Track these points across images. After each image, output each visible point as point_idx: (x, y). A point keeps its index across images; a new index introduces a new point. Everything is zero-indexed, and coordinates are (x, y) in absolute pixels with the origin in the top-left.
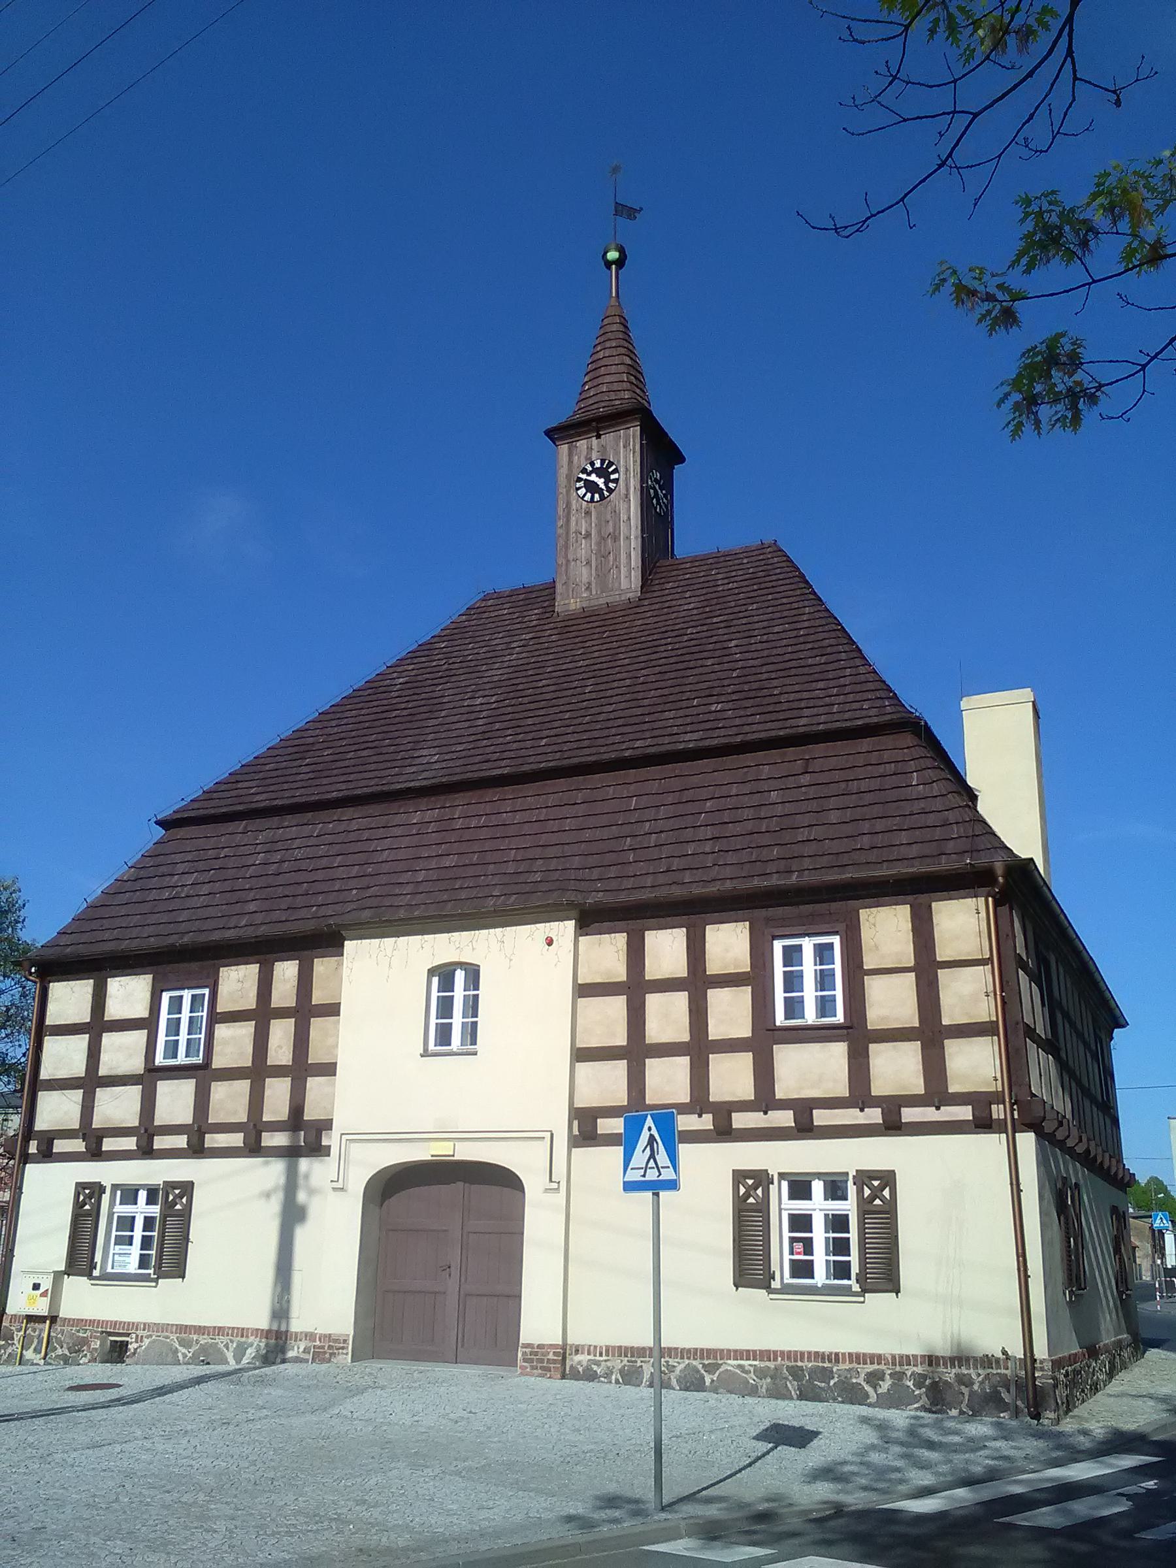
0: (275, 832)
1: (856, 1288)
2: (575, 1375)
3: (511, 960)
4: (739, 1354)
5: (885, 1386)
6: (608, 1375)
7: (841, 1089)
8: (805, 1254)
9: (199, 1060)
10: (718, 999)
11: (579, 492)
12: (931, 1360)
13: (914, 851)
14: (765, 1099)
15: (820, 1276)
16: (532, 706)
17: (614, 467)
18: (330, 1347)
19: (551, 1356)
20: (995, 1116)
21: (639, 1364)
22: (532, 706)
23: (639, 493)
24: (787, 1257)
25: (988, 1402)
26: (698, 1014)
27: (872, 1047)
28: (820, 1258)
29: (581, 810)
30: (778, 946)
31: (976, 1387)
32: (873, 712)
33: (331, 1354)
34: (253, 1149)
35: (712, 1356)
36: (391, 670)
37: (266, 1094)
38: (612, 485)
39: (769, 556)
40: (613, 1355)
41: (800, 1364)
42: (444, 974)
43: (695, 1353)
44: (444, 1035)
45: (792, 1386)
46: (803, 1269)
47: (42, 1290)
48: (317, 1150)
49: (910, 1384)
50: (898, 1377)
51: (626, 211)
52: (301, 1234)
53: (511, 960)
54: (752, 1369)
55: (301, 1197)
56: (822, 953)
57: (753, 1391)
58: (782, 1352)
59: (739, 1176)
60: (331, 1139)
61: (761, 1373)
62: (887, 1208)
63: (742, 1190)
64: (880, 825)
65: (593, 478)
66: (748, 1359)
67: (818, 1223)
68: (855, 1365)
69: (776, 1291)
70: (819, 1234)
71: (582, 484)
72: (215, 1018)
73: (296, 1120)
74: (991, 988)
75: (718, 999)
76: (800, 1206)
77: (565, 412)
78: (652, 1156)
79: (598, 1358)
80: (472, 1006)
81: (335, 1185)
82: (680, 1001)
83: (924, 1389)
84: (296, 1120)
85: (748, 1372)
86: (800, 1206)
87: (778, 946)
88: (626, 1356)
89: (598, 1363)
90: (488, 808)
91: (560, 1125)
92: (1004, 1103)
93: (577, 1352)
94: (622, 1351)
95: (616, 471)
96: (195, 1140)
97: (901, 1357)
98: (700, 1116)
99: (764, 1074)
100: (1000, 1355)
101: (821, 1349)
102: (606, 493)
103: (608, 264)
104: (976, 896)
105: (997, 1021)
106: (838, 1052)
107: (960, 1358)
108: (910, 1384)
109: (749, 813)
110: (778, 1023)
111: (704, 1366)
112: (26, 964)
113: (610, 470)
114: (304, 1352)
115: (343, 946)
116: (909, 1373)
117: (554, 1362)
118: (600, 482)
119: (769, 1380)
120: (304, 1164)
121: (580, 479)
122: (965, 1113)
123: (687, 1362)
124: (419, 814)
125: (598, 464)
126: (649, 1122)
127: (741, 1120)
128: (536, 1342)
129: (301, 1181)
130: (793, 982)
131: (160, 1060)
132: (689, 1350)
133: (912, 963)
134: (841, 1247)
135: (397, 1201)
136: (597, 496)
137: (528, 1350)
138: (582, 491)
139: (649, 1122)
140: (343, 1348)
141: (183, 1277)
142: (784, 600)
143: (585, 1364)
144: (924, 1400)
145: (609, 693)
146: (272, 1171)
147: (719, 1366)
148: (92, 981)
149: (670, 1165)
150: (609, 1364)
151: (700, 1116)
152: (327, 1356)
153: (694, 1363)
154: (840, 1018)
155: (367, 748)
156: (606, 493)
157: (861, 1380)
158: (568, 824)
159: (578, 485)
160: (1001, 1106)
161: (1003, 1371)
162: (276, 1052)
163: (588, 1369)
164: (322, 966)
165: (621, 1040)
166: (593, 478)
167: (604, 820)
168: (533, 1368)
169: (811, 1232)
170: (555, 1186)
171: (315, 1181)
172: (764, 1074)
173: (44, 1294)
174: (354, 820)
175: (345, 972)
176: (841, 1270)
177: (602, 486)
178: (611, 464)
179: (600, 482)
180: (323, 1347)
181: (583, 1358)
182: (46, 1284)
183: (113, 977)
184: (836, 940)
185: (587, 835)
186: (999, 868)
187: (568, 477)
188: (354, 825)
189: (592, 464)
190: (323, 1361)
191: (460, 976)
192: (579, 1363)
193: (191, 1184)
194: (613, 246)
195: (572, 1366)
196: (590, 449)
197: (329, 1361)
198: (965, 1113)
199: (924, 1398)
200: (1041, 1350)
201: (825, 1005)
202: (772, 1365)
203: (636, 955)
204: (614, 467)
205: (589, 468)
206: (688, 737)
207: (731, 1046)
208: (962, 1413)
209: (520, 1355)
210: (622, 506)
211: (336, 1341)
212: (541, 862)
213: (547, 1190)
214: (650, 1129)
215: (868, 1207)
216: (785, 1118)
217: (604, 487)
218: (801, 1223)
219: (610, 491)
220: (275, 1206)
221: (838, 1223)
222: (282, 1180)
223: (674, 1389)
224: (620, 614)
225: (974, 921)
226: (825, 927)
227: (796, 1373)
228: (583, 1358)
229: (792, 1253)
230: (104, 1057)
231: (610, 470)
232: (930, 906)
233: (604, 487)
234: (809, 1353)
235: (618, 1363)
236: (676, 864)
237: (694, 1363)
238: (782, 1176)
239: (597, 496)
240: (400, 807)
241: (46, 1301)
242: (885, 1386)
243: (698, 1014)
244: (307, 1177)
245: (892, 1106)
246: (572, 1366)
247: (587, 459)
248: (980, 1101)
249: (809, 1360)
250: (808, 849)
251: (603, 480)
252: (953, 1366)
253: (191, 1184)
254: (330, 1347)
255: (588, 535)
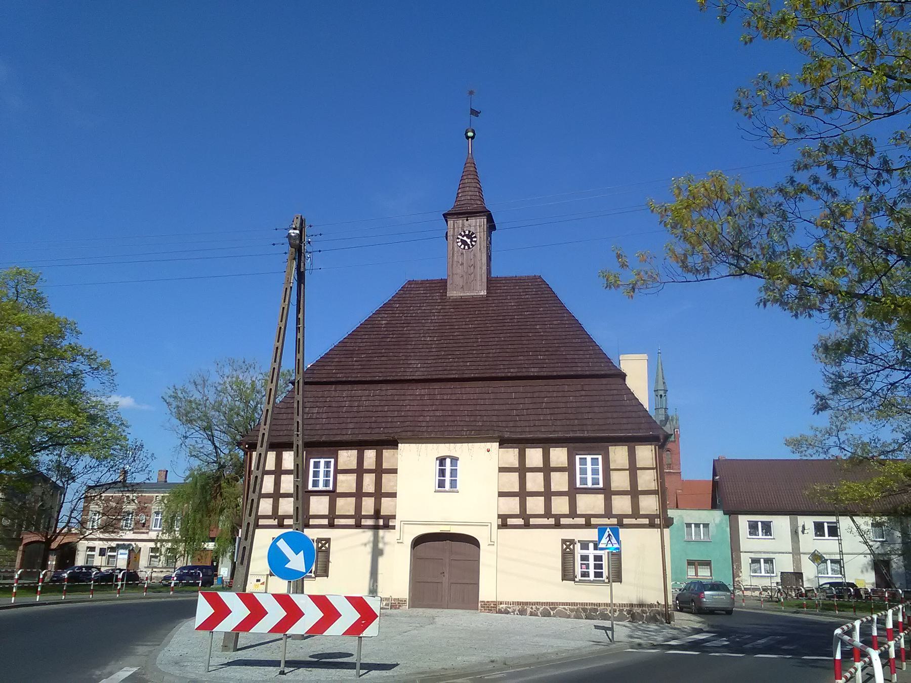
0: (351, 392)
1: (313, 576)
2: (500, 612)
3: (472, 456)
4: (563, 604)
5: (617, 614)
6: (514, 612)
7: (601, 511)
8: (586, 569)
9: (331, 488)
10: (555, 476)
11: (458, 244)
12: (632, 605)
13: (629, 426)
14: (573, 513)
15: (592, 577)
16: (455, 345)
17: (474, 235)
18: (398, 603)
19: (492, 605)
20: (656, 523)
21: (525, 608)
22: (455, 345)
23: (486, 249)
24: (580, 570)
25: (653, 619)
26: (547, 481)
27: (613, 497)
28: (592, 571)
29: (492, 396)
30: (578, 457)
31: (648, 614)
32: (606, 368)
33: (399, 606)
34: (358, 526)
35: (553, 605)
36: (376, 316)
37: (363, 503)
38: (473, 243)
39: (540, 283)
40: (515, 605)
41: (586, 607)
42: (442, 461)
43: (547, 604)
44: (441, 484)
45: (583, 615)
46: (585, 574)
47: (261, 582)
48: (386, 527)
49: (625, 613)
50: (621, 611)
51: (474, 113)
52: (381, 560)
53: (472, 456)
54: (568, 609)
55: (381, 545)
56: (595, 462)
57: (569, 617)
58: (579, 603)
59: (564, 541)
60: (396, 523)
61: (572, 611)
62: (571, 552)
63: (565, 547)
64: (615, 415)
65: (465, 238)
66: (567, 605)
67: (591, 559)
68: (606, 607)
69: (577, 582)
70: (592, 562)
71: (460, 240)
72: (337, 471)
73: (377, 515)
74: (656, 478)
75: (555, 476)
76: (585, 552)
77: (449, 207)
78: (610, 540)
79: (509, 606)
80: (454, 473)
81: (399, 541)
82: (540, 476)
83: (630, 615)
84: (377, 515)
85: (567, 610)
86: (585, 552)
87: (578, 457)
88: (520, 605)
89: (510, 608)
90: (449, 391)
91: (496, 522)
92: (660, 518)
93: (501, 604)
94: (519, 603)
95: (475, 237)
96: (331, 522)
97: (622, 604)
98: (548, 519)
99: (573, 505)
100: (656, 604)
101: (593, 602)
102: (471, 247)
103: (468, 138)
104: (651, 445)
105: (658, 490)
106: (601, 497)
107: (641, 605)
108: (625, 613)
109: (562, 405)
110: (578, 486)
111: (550, 608)
112: (244, 444)
113: (473, 236)
114: (385, 605)
115: (398, 446)
116: (625, 610)
117: (493, 607)
118: (468, 241)
119: (575, 613)
120: (381, 532)
121: (458, 238)
122: (646, 521)
123: (544, 607)
124: (419, 390)
125: (467, 233)
126: (608, 530)
127: (563, 521)
128: (486, 601)
129: (380, 539)
130: (584, 471)
131: (310, 487)
132: (545, 603)
133: (628, 468)
134: (598, 566)
135: (420, 547)
136: (466, 247)
137: (483, 603)
138: (460, 244)
139: (608, 530)
140: (404, 603)
141: (328, 576)
142: (554, 308)
143: (504, 608)
144: (630, 619)
145: (490, 344)
146: (368, 535)
147: (556, 608)
148: (275, 452)
149: (616, 542)
150: (514, 608)
151: (548, 519)
152: (398, 606)
153: (547, 607)
154: (601, 485)
155: (383, 356)
156: (471, 247)
157: (608, 612)
158: (487, 402)
159: (458, 240)
160: (659, 519)
161: (657, 609)
162: (367, 487)
163: (506, 610)
164: (387, 453)
165: (517, 489)
166: (465, 238)
167: (502, 402)
168: (485, 610)
169: (588, 561)
170: (493, 543)
171: (387, 539)
172: (573, 505)
173: (263, 584)
174: (390, 391)
175: (399, 456)
176: (598, 575)
177: (469, 243)
178: (473, 234)
179: (468, 241)
180: (395, 603)
181: (504, 606)
182: (263, 579)
183: (286, 451)
184: (600, 457)
185: (497, 407)
186: (661, 437)
187: (453, 236)
188: (389, 393)
189: (464, 232)
190: (396, 608)
191: (448, 461)
192: (502, 608)
193: (330, 539)
194: (470, 130)
195: (499, 609)
196: (463, 225)
197: (399, 608)
198: (646, 521)
199: (630, 618)
200: (670, 602)
201: (595, 482)
202: (576, 607)
203: (522, 457)
204: (474, 235)
205: (463, 233)
206: (533, 370)
207: (560, 494)
208: (643, 623)
209: (479, 605)
210: (478, 255)
211: (401, 601)
212: (479, 417)
213: (489, 545)
214: (608, 532)
215: (565, 552)
216: (582, 521)
217: (470, 244)
218: (585, 558)
219: (472, 245)
220: (369, 548)
221: (598, 558)
222: (372, 539)
223: (539, 616)
224: (478, 303)
225: (651, 454)
226: (597, 452)
227: (585, 610)
228: (504, 606)
229: (581, 569)
230: (282, 485)
231: (473, 236)
232: (635, 447)
233: (470, 244)
234: (589, 603)
235: (517, 608)
236: (537, 423)
237: (547, 607)
238: (579, 541)
239: (466, 247)
240: (408, 386)
241: (264, 586)
242: (617, 614)
243: (547, 481)
244: (383, 538)
245: (558, 517)
246: (499, 609)
247: (462, 229)
248: (651, 517)
249: (589, 605)
250: (589, 422)
251: (469, 240)
252: (640, 607)
253: (330, 539)
254: (398, 603)
255: (462, 264)
